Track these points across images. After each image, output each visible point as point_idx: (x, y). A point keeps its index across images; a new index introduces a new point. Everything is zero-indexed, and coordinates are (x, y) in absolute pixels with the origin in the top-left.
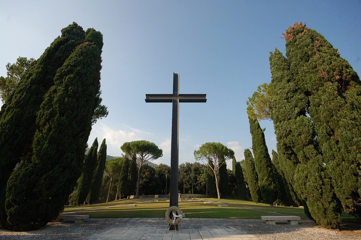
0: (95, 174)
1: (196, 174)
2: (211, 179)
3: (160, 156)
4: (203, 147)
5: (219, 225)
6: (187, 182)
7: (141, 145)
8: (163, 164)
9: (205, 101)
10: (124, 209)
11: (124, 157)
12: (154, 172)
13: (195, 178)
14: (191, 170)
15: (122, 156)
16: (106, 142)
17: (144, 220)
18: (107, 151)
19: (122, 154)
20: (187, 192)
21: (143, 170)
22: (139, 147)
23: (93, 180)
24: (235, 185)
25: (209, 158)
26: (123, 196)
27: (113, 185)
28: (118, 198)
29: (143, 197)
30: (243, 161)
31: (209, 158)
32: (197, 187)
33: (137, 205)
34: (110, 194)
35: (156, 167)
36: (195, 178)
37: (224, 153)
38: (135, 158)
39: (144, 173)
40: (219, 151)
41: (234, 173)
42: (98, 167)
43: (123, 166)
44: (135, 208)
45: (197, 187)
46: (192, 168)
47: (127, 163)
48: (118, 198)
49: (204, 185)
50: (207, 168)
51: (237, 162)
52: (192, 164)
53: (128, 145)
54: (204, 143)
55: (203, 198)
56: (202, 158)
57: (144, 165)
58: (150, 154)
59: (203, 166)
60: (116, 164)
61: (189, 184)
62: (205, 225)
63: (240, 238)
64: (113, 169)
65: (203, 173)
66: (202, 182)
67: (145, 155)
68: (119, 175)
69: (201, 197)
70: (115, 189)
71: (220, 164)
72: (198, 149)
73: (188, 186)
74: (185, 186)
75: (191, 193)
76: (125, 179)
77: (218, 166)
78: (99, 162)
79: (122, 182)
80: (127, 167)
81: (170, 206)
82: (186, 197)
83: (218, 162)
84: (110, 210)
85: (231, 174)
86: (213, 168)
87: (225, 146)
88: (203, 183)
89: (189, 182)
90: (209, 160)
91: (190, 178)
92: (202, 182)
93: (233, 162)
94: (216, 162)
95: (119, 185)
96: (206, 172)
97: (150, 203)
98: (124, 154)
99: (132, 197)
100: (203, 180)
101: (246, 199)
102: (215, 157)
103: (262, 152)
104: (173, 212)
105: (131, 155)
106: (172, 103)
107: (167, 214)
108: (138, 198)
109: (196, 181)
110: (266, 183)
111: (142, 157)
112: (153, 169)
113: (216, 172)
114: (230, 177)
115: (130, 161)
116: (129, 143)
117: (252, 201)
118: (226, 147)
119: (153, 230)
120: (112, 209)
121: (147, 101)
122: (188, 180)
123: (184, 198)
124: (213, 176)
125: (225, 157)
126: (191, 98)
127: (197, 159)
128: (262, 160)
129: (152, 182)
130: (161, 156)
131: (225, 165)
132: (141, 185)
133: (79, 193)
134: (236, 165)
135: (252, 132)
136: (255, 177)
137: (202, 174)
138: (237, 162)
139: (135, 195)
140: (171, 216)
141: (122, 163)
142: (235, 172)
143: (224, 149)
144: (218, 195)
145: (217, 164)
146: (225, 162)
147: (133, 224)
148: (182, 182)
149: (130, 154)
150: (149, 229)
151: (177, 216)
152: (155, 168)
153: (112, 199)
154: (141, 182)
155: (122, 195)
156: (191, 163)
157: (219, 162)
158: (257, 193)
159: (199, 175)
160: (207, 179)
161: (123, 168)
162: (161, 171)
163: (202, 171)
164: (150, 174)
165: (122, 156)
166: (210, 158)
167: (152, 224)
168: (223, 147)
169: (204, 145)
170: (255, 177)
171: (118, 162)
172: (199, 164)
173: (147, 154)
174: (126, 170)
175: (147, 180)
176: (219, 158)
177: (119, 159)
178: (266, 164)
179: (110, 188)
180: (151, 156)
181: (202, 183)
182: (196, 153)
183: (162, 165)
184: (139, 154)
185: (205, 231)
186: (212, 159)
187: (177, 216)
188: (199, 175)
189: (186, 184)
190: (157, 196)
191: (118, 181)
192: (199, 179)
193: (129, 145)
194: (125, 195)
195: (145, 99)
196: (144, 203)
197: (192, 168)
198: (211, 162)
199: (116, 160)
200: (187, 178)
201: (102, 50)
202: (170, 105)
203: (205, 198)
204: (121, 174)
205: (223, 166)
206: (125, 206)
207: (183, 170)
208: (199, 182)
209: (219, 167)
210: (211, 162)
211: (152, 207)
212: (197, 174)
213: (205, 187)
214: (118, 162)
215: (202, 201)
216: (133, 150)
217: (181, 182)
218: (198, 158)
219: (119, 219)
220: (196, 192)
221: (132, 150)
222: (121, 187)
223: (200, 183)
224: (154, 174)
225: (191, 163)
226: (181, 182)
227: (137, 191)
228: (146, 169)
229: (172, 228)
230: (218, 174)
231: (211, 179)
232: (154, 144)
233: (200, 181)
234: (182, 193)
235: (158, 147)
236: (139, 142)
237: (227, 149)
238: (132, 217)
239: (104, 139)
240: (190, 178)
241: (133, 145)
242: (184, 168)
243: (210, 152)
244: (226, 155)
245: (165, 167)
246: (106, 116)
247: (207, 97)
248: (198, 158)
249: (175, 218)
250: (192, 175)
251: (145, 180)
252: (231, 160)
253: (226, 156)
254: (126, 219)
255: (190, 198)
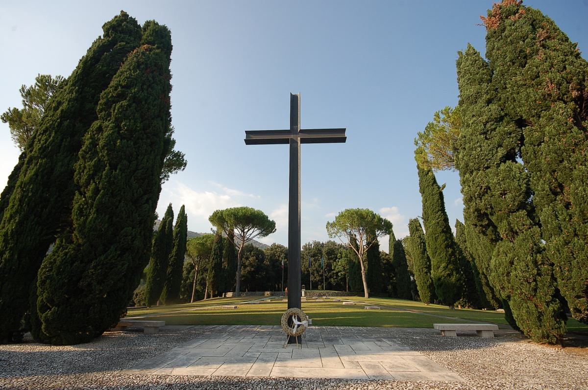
0: (172, 259)
1: (329, 259)
2: (354, 267)
3: (271, 232)
4: (342, 216)
5: (366, 337)
6: (315, 272)
7: (240, 214)
8: (277, 244)
9: (343, 140)
10: (218, 313)
11: (214, 233)
12: (263, 257)
13: (329, 266)
14: (321, 254)
15: (212, 233)
16: (185, 210)
17: (249, 328)
18: (188, 224)
19: (212, 229)
20: (315, 287)
21: (245, 254)
22: (237, 218)
23: (169, 270)
24: (394, 277)
25: (351, 234)
26: (216, 293)
27: (200, 277)
28: (209, 297)
29: (247, 295)
30: (406, 239)
31: (351, 234)
32: (332, 280)
33: (238, 306)
34: (196, 290)
35: (265, 249)
36: (329, 266)
37: (376, 225)
38: (231, 235)
39: (247, 258)
40: (367, 223)
41: (391, 257)
42: (175, 250)
43: (213, 247)
44: (235, 310)
45: (332, 280)
46: (324, 250)
47: (220, 243)
48: (209, 297)
49: (342, 276)
50: (347, 250)
51: (397, 240)
52: (322, 244)
53: (219, 215)
54: (343, 210)
55: (341, 296)
56: (339, 234)
57: (246, 246)
58: (256, 229)
59: (341, 246)
60: (203, 244)
61: (319, 274)
62: (344, 337)
63: (398, 356)
64: (199, 251)
65: (341, 257)
66: (340, 271)
67: (249, 230)
68: (209, 261)
69: (337, 295)
70: (203, 283)
71: (368, 244)
72: (332, 220)
73: (318, 278)
74: (312, 278)
75: (323, 289)
76: (217, 267)
77: (365, 247)
78: (176, 242)
79: (213, 272)
80: (221, 249)
81: (289, 308)
82: (314, 294)
83: (365, 241)
84: (197, 313)
85: (387, 260)
86: (358, 250)
87: (377, 214)
88: (341, 274)
89: (318, 272)
90: (351, 238)
91: (320, 265)
92: (340, 271)
93: (390, 240)
94: (362, 241)
95: (209, 277)
96: (346, 256)
97: (257, 304)
98: (215, 228)
99: (230, 294)
100: (341, 268)
101: (410, 298)
102: (361, 231)
103: (438, 223)
104: (293, 317)
105: (225, 231)
106: (289, 145)
107: (284, 321)
108: (239, 296)
109: (330, 270)
110: (443, 273)
111: (244, 233)
112: (261, 252)
113: (362, 256)
114: (385, 264)
115: (225, 239)
116: (222, 212)
117: (420, 301)
118: (380, 216)
119: (262, 344)
120: (200, 311)
121: (248, 142)
122: (316, 269)
123: (311, 296)
124: (356, 262)
125: (377, 233)
126: (330, 135)
127: (330, 235)
128: (438, 236)
129: (260, 273)
130: (274, 232)
131: (377, 246)
132: (243, 276)
133: (149, 288)
134: (395, 245)
135: (422, 191)
136: (426, 263)
137: (339, 259)
138: (397, 240)
139: (234, 291)
140: (290, 323)
141: (212, 243)
142: (393, 255)
143: (376, 220)
144: (364, 292)
145: (364, 243)
146: (376, 240)
147: (233, 334)
148: (308, 271)
149: (225, 229)
150: (257, 341)
151: (299, 323)
152: (264, 251)
153: (199, 297)
154: (242, 273)
155: (214, 292)
156: (321, 243)
157: (367, 239)
158: (428, 288)
159: (335, 261)
160: (347, 267)
161: (215, 250)
162: (274, 255)
163: (339, 255)
164: (257, 259)
165: (212, 233)
166: (352, 233)
167: (261, 335)
168: (374, 216)
169: (342, 213)
170: (426, 263)
171: (206, 241)
172: (334, 244)
173: (250, 229)
174: (219, 255)
175: (252, 269)
176: (367, 234)
177: (207, 237)
178: (444, 242)
179: (196, 281)
180: (257, 232)
181: (339, 274)
182: (330, 225)
183: (275, 245)
184: (238, 229)
185: (344, 346)
186: (355, 235)
187: (299, 323)
188: (335, 261)
189: (314, 275)
190: (269, 293)
191: (207, 270)
192: (335, 267)
193: (222, 215)
194: (219, 292)
195: (245, 139)
196: (249, 304)
197: (324, 250)
198: (353, 240)
199: (203, 238)
200: (316, 265)
201: (171, 57)
202: (286, 147)
203: (344, 296)
204: (211, 260)
205: (373, 247)
206: (220, 308)
207: (309, 253)
208: (335, 272)
209: (367, 248)
210: (353, 240)
211: (261, 310)
212: (331, 259)
213: (344, 279)
214: (206, 241)
215: (339, 301)
216: (229, 222)
217: (306, 272)
218: (334, 235)
219: (211, 327)
220: (330, 287)
221: (227, 222)
222: (211, 280)
223: (337, 273)
224: (262, 260)
225: (321, 243)
226: (306, 272)
227: (237, 285)
228: (251, 251)
229: (292, 340)
230: (365, 260)
231: (354, 267)
232: (262, 213)
233: (337, 270)
234: (307, 288)
235: (267, 217)
236: (237, 210)
237: (380, 220)
238: (230, 324)
239: (182, 205)
240: (320, 265)
241: (228, 215)
242: (310, 249)
243: (352, 225)
244: (379, 229)
245: (281, 248)
246: (184, 169)
247: (244, 136)
248: (334, 235)
249: (296, 326)
250: (324, 261)
251: (248, 268)
252: (388, 236)
253: (379, 231)
254: (221, 326)
255: (320, 296)
